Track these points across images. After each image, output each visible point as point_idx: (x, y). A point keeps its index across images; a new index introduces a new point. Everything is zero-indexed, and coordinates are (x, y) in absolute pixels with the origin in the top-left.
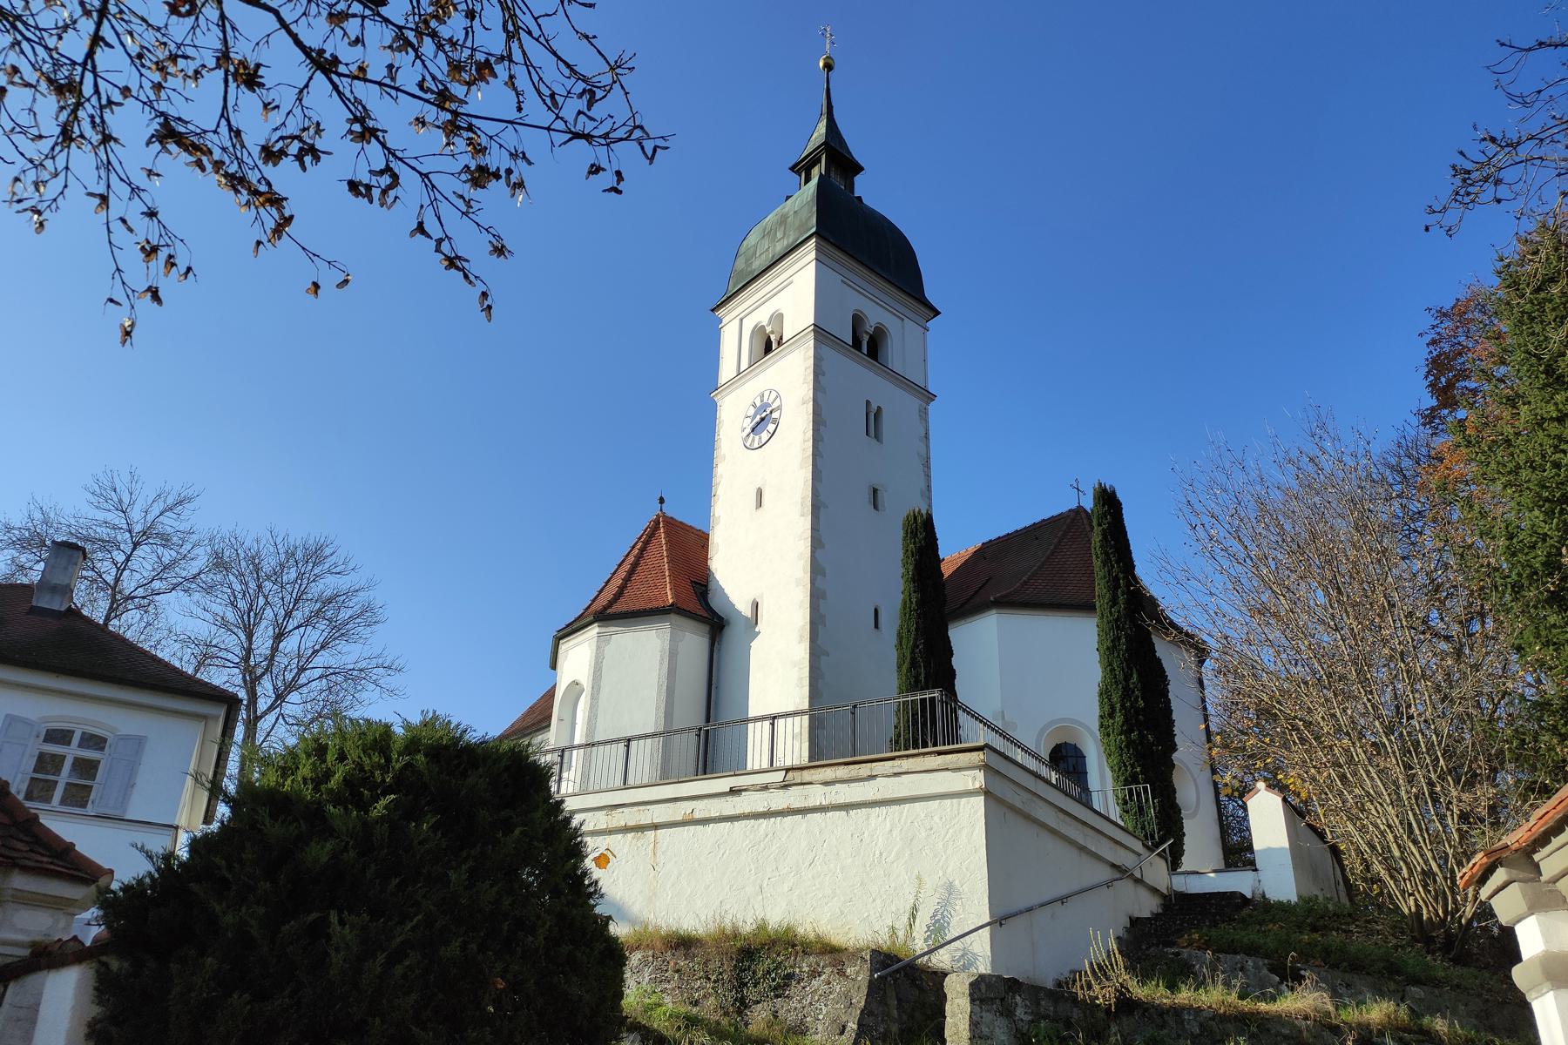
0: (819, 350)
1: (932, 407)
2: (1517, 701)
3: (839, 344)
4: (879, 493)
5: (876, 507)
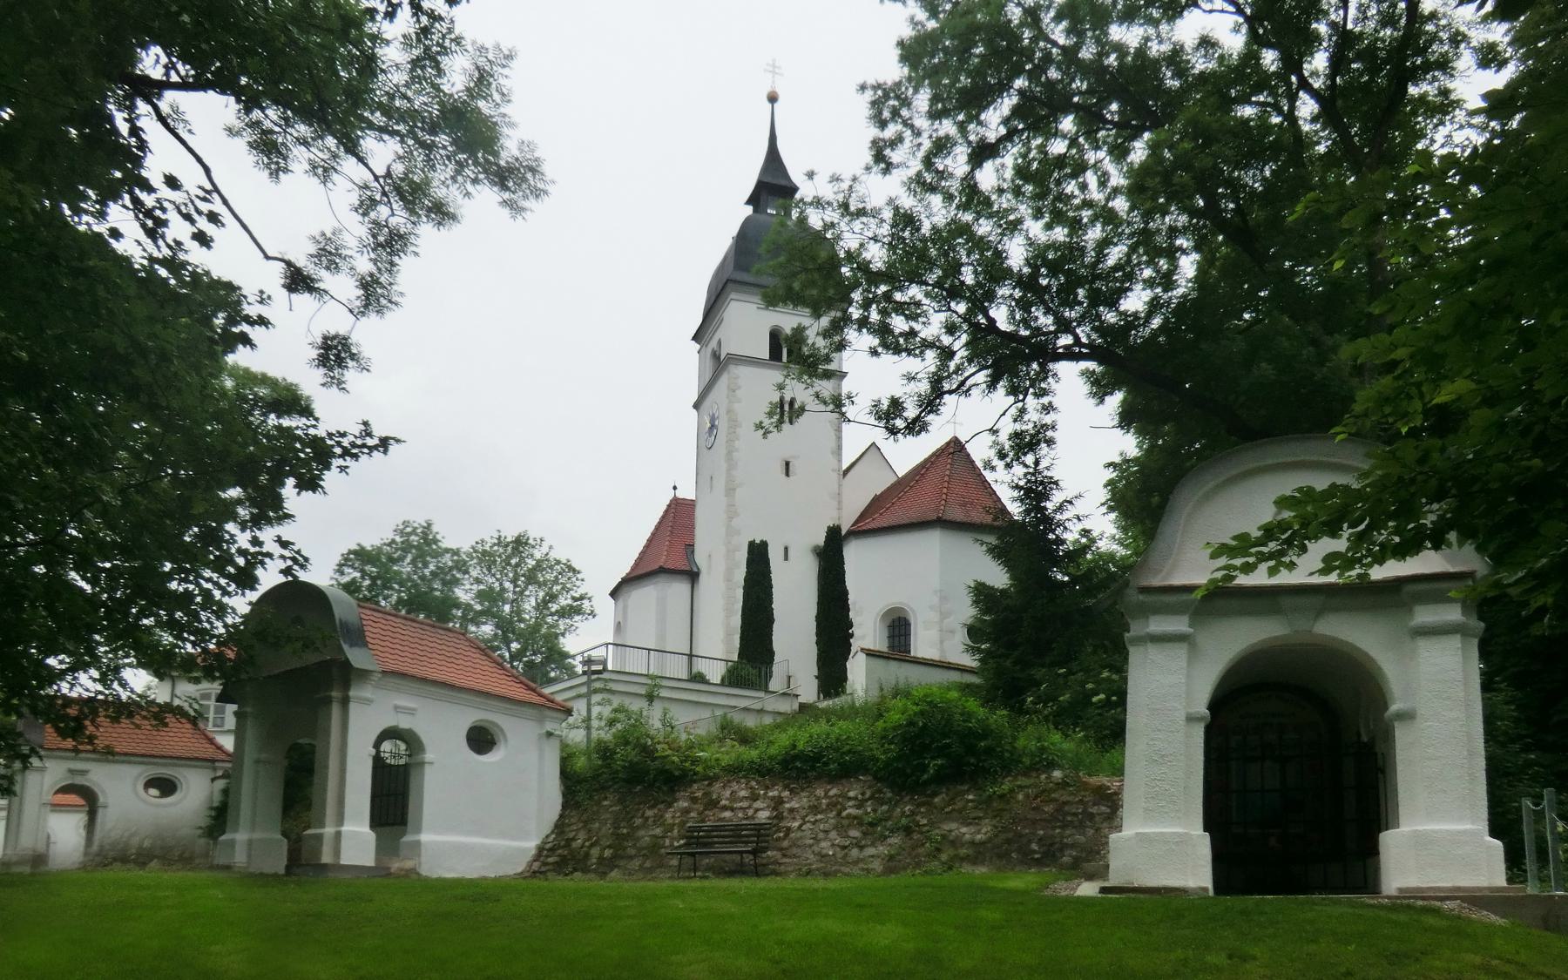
5: (787, 474)
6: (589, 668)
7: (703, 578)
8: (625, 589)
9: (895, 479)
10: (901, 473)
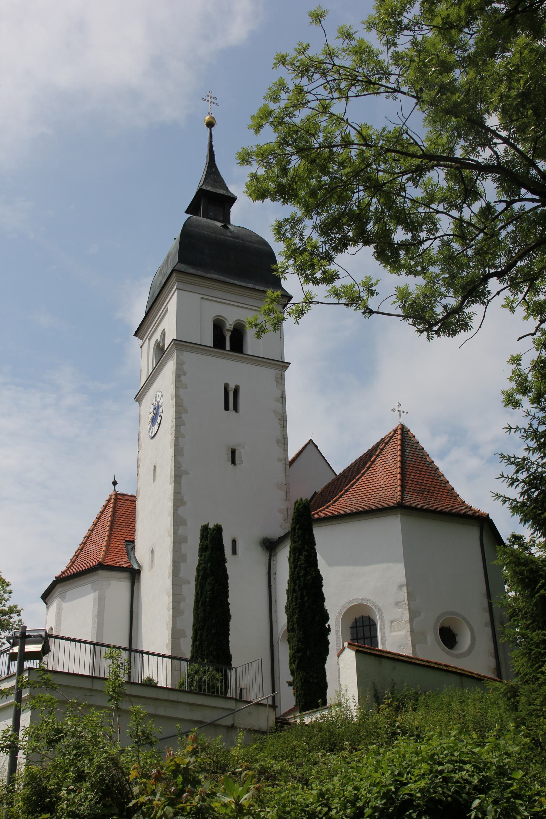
0: (181, 357)
1: (288, 373)
2: (483, 57)
3: (204, 349)
4: (237, 453)
5: (233, 462)
6: (22, 649)
7: (145, 576)
8: (59, 589)
9: (334, 477)
10: (339, 471)
